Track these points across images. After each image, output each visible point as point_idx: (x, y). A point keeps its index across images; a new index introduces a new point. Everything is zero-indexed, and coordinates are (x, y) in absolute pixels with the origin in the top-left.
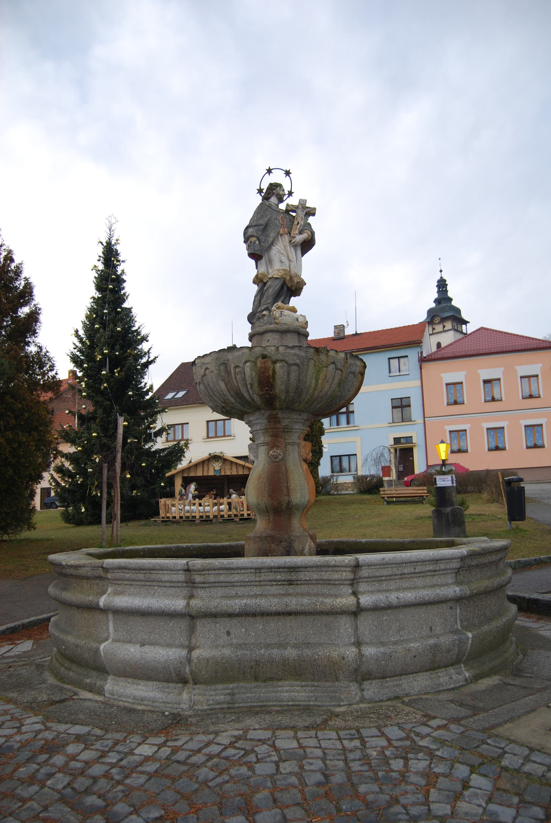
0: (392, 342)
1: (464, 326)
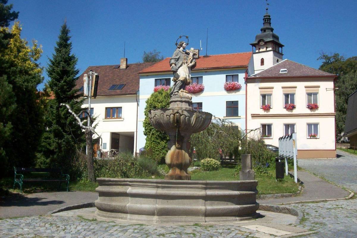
0: (228, 65)
1: (280, 49)
